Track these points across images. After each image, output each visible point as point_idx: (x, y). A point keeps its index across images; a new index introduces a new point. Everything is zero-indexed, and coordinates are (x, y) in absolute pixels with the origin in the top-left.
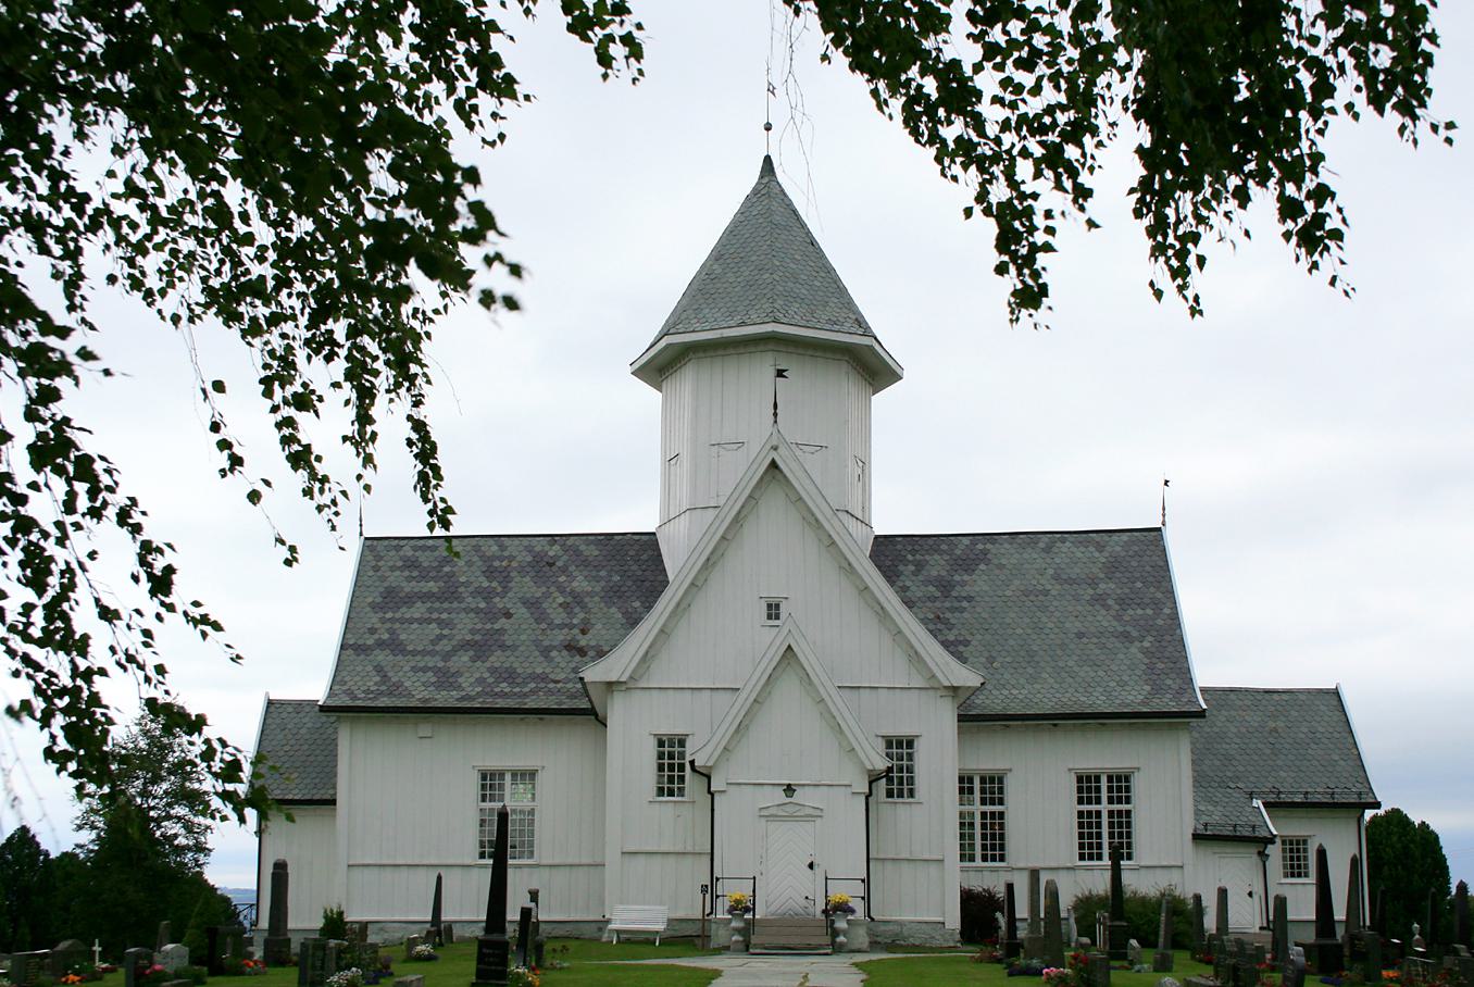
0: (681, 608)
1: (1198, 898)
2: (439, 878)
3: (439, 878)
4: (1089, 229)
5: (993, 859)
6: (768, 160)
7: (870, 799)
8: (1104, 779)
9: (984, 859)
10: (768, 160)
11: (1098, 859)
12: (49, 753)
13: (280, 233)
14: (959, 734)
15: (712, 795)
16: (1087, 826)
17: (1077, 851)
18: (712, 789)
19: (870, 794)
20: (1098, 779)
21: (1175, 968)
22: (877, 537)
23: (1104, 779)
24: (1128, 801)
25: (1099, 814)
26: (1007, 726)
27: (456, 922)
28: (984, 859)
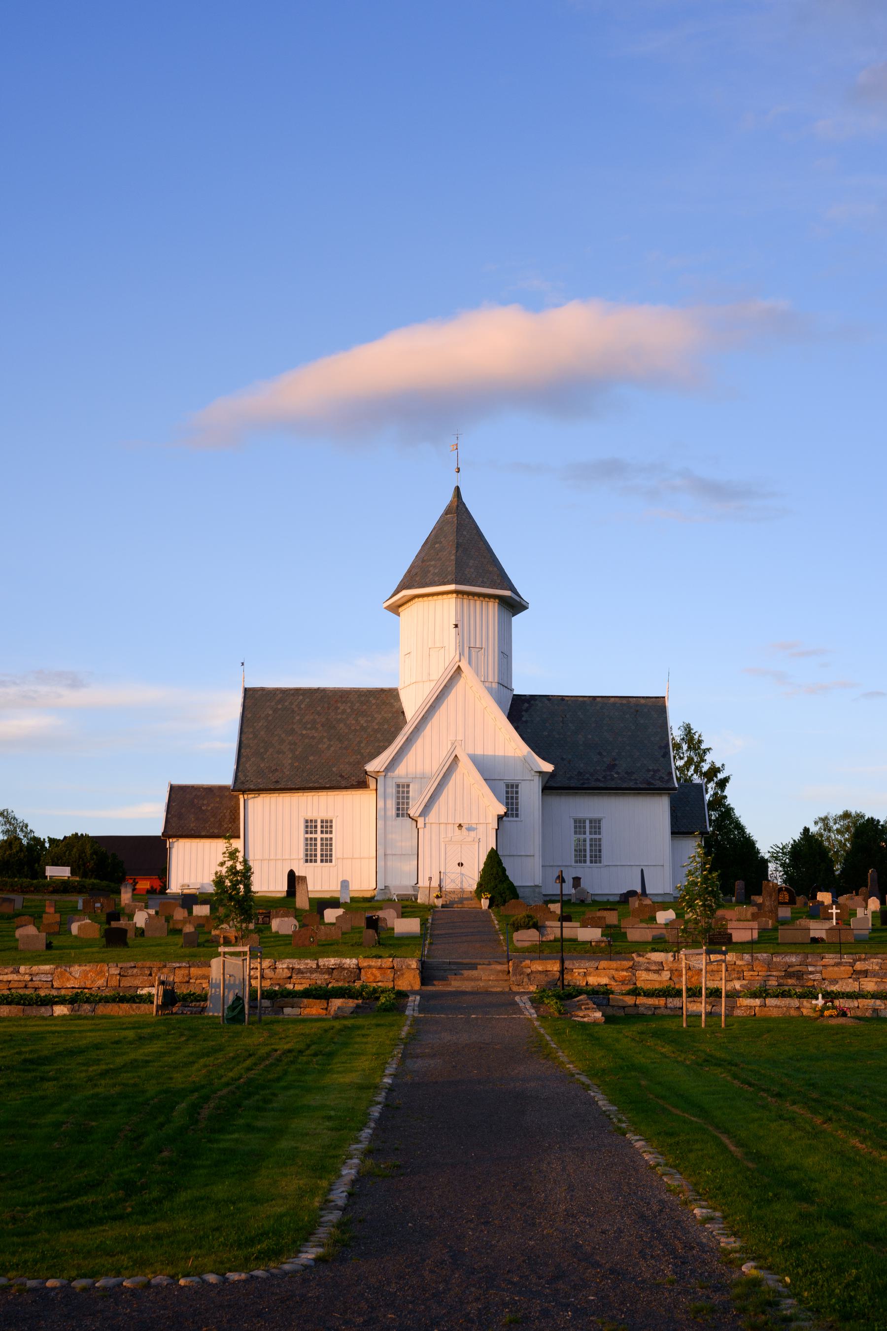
0: (409, 741)
1: (44, 839)
2: (642, 871)
3: (642, 871)
4: (398, 615)
5: (596, 862)
6: (457, 489)
7: (498, 831)
8: (587, 822)
9: (591, 862)
10: (457, 489)
11: (584, 863)
12: (34, 832)
13: (10, 825)
14: (542, 795)
15: (418, 829)
16: (310, 844)
17: (334, 824)
18: (418, 827)
19: (498, 829)
20: (584, 822)
21: (681, 987)
22: (514, 695)
23: (587, 822)
24: (600, 834)
25: (316, 839)
26: (576, 793)
27: (749, 921)
28: (591, 862)
